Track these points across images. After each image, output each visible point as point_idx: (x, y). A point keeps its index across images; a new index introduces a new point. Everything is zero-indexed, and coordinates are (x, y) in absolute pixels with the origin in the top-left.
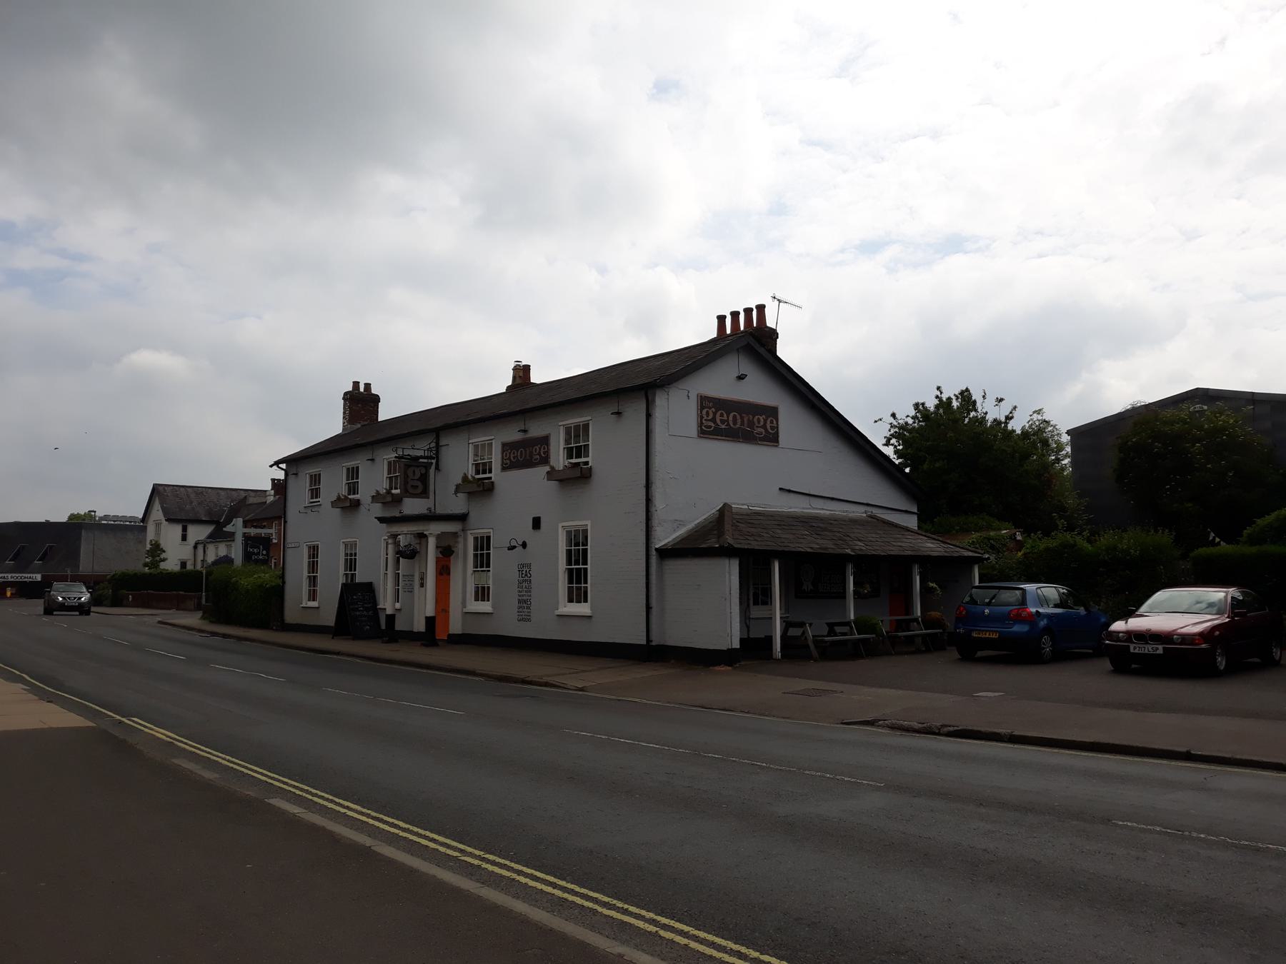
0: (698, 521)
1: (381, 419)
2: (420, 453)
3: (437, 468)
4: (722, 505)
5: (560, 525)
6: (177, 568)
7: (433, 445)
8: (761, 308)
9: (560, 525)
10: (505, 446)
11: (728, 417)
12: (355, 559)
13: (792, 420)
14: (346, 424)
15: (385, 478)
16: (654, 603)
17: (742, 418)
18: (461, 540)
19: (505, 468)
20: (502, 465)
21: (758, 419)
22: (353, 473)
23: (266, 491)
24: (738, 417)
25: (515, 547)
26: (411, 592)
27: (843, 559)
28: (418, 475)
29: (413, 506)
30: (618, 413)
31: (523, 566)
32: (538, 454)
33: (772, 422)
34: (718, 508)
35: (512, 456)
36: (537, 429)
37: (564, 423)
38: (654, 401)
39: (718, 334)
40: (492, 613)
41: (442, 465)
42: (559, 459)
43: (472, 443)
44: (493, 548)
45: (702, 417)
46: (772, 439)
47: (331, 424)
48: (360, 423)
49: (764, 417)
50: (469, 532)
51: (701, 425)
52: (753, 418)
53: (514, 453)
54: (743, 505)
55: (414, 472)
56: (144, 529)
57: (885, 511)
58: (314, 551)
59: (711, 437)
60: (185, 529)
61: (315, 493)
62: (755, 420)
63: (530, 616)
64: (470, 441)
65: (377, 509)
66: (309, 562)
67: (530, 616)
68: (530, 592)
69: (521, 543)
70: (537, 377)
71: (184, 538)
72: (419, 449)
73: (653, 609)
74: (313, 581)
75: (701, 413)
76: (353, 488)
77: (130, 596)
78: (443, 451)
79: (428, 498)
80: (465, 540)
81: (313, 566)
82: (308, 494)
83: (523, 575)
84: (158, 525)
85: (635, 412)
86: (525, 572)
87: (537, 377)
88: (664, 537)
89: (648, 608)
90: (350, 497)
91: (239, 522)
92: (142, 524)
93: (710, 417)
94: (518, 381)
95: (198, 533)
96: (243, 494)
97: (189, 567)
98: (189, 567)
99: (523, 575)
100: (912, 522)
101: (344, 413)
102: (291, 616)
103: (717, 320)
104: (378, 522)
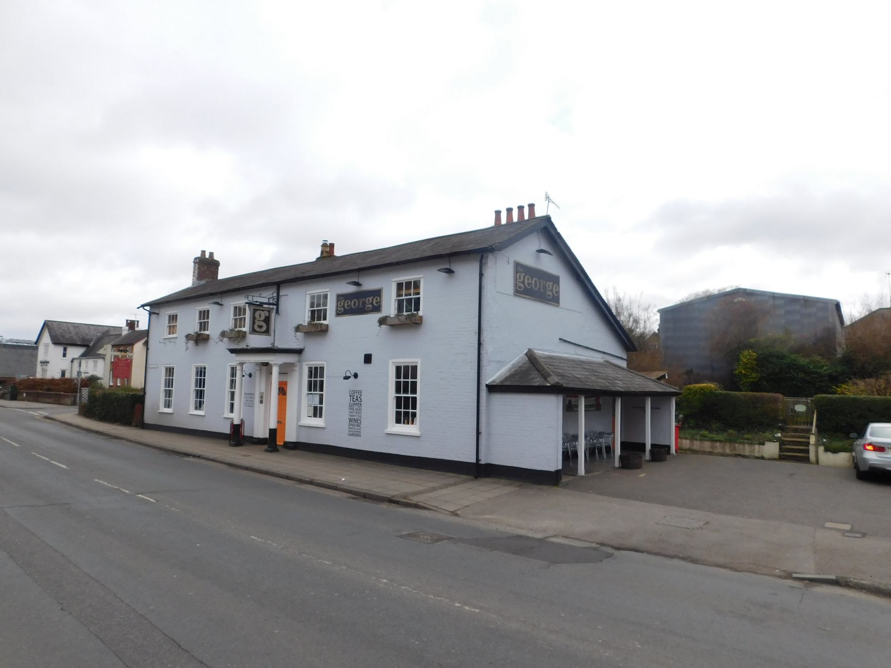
0: (512, 363)
1: (219, 278)
2: (266, 300)
3: (277, 312)
4: (527, 350)
5: (391, 361)
6: (58, 376)
7: (275, 295)
8: (531, 206)
9: (391, 361)
10: (340, 297)
11: (532, 281)
12: (204, 379)
13: (568, 289)
14: (195, 280)
15: (231, 319)
16: (483, 429)
17: (540, 283)
18: (297, 369)
19: (338, 314)
20: (337, 312)
21: (549, 284)
22: (204, 314)
23: (121, 328)
24: (357, 301)
25: (349, 377)
26: (252, 406)
27: (614, 394)
28: (263, 318)
29: (256, 341)
30: (450, 271)
31: (354, 392)
32: (371, 304)
33: (556, 288)
34: (525, 352)
35: (346, 304)
36: (370, 283)
37: (233, 303)
38: (487, 263)
39: (529, 217)
40: (325, 428)
41: (280, 309)
42: (390, 307)
43: (309, 294)
44: (327, 377)
45: (516, 280)
46: (554, 300)
47: (186, 281)
48: (205, 280)
49: (552, 283)
50: (304, 363)
51: (516, 285)
52: (546, 283)
53: (348, 303)
54: (538, 350)
55: (260, 315)
56: (35, 348)
57: (615, 358)
58: (170, 371)
59: (522, 295)
60: (65, 350)
61: (172, 329)
62: (367, 301)
63: (360, 432)
64: (307, 293)
65: (226, 344)
66: (166, 379)
67: (360, 432)
68: (360, 413)
69: (353, 374)
70: (338, 252)
71: (64, 355)
72: (264, 297)
73: (482, 434)
74: (169, 394)
75: (516, 275)
76: (204, 326)
77: (25, 394)
78: (283, 301)
79: (270, 335)
80: (301, 369)
81: (169, 383)
82: (167, 330)
83: (354, 400)
84: (47, 346)
85: (467, 272)
86: (356, 399)
87: (338, 252)
88: (493, 375)
89: (478, 433)
90: (236, 329)
91: (109, 347)
92: (35, 345)
93: (521, 280)
94: (325, 255)
95: (75, 352)
96: (107, 329)
97: (67, 376)
98: (67, 376)
99: (354, 400)
100: (624, 364)
101: (194, 272)
102: (148, 418)
103: (517, 209)
104: (229, 353)
